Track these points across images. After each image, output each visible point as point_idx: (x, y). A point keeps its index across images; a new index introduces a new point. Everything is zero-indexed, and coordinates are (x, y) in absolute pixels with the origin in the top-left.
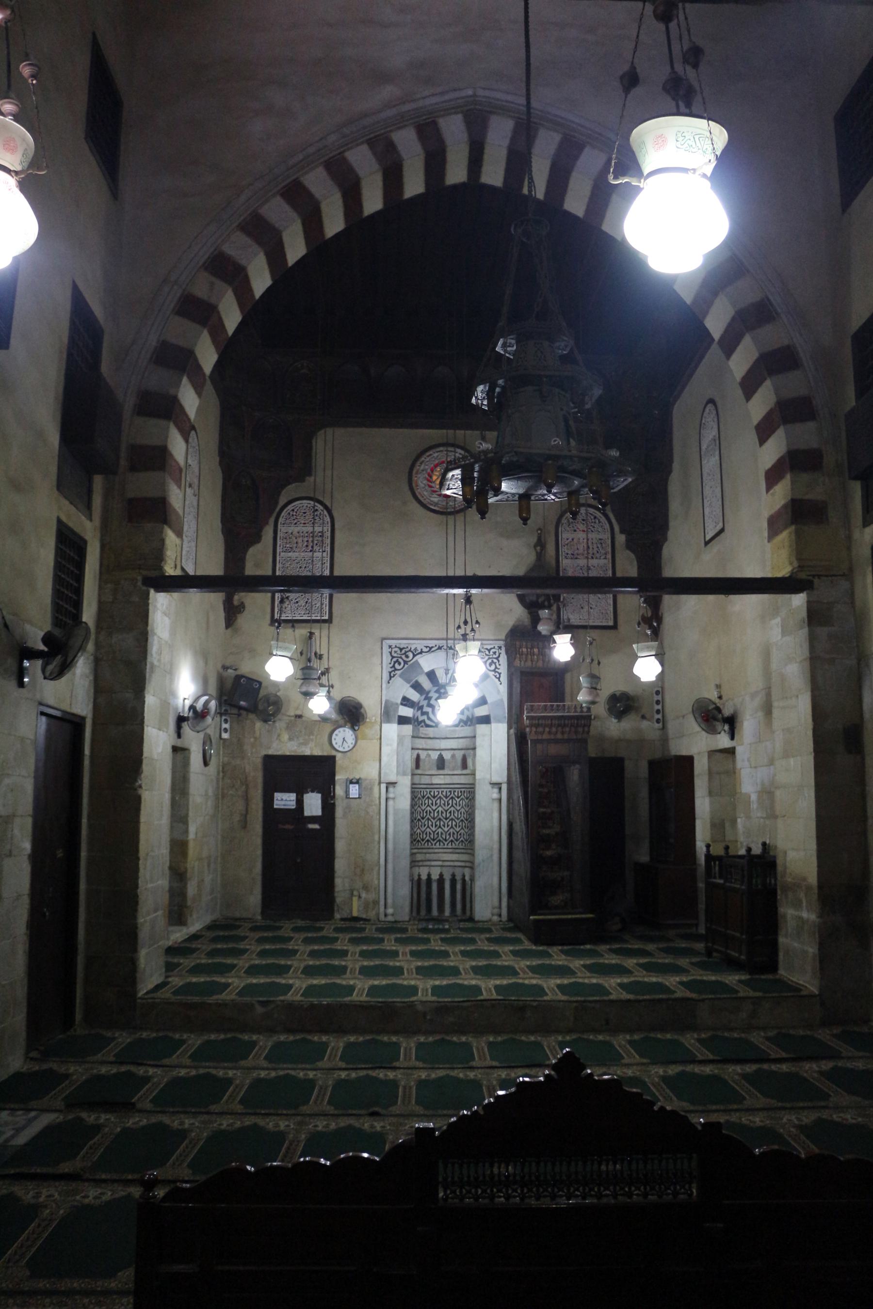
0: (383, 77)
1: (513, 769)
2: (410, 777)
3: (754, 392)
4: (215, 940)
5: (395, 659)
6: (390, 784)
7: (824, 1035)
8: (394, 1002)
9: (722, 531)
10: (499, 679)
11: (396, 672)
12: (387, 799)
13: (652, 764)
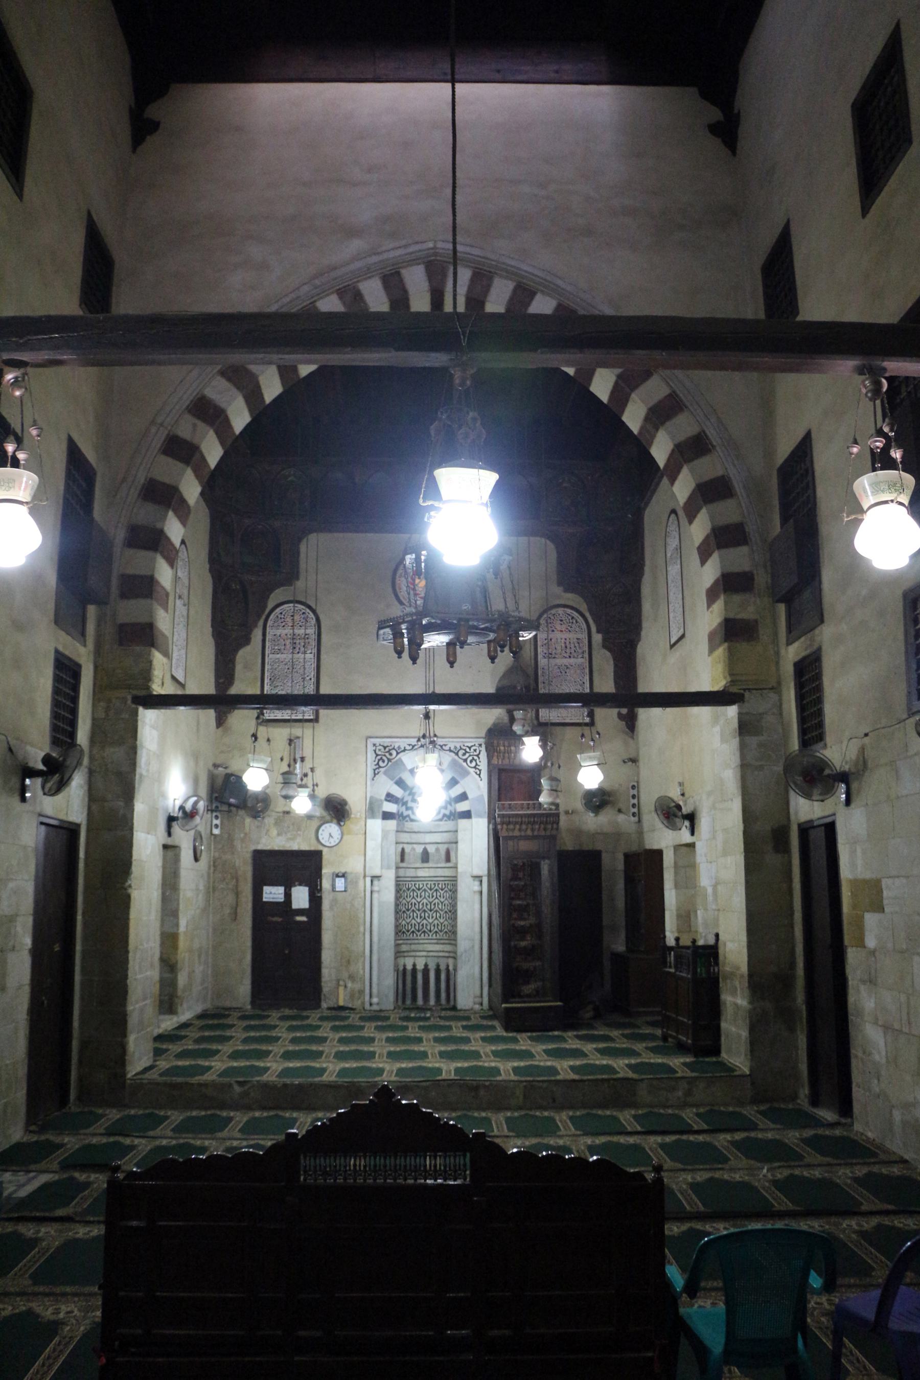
0: (352, 232)
1: (491, 864)
2: (394, 871)
3: (695, 517)
4: (202, 1028)
5: (379, 757)
6: (375, 878)
7: (750, 1111)
8: (358, 1082)
9: (683, 636)
10: (479, 775)
11: (381, 769)
12: (372, 892)
13: (627, 856)
